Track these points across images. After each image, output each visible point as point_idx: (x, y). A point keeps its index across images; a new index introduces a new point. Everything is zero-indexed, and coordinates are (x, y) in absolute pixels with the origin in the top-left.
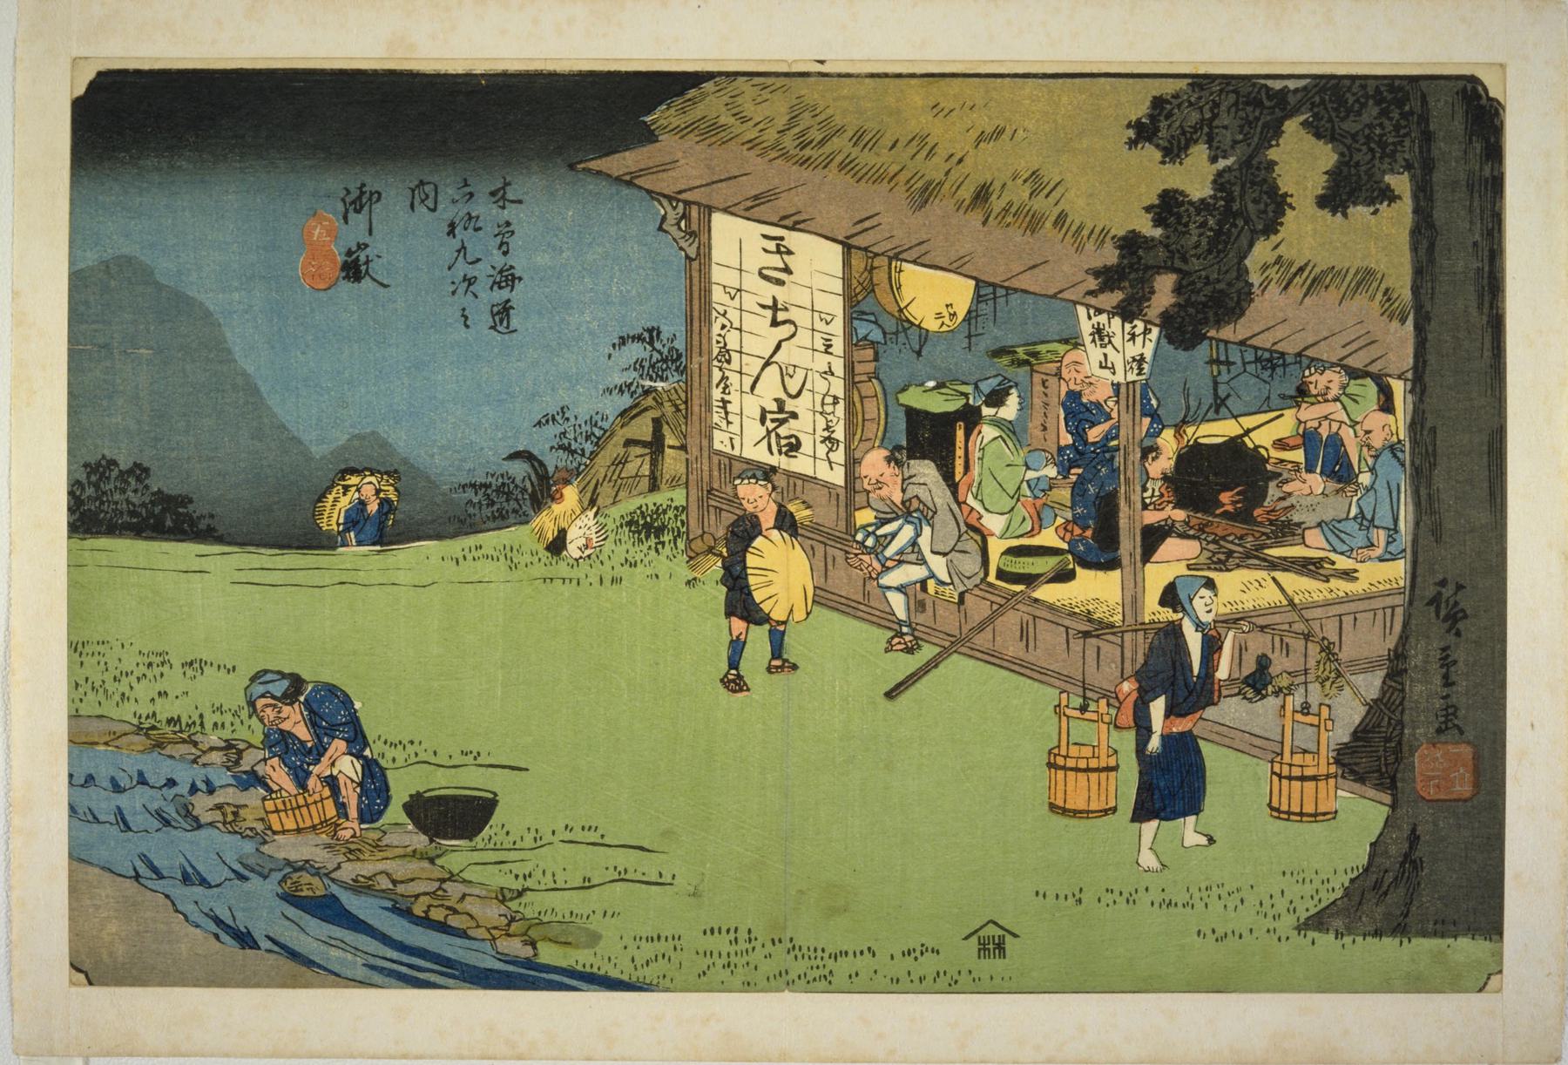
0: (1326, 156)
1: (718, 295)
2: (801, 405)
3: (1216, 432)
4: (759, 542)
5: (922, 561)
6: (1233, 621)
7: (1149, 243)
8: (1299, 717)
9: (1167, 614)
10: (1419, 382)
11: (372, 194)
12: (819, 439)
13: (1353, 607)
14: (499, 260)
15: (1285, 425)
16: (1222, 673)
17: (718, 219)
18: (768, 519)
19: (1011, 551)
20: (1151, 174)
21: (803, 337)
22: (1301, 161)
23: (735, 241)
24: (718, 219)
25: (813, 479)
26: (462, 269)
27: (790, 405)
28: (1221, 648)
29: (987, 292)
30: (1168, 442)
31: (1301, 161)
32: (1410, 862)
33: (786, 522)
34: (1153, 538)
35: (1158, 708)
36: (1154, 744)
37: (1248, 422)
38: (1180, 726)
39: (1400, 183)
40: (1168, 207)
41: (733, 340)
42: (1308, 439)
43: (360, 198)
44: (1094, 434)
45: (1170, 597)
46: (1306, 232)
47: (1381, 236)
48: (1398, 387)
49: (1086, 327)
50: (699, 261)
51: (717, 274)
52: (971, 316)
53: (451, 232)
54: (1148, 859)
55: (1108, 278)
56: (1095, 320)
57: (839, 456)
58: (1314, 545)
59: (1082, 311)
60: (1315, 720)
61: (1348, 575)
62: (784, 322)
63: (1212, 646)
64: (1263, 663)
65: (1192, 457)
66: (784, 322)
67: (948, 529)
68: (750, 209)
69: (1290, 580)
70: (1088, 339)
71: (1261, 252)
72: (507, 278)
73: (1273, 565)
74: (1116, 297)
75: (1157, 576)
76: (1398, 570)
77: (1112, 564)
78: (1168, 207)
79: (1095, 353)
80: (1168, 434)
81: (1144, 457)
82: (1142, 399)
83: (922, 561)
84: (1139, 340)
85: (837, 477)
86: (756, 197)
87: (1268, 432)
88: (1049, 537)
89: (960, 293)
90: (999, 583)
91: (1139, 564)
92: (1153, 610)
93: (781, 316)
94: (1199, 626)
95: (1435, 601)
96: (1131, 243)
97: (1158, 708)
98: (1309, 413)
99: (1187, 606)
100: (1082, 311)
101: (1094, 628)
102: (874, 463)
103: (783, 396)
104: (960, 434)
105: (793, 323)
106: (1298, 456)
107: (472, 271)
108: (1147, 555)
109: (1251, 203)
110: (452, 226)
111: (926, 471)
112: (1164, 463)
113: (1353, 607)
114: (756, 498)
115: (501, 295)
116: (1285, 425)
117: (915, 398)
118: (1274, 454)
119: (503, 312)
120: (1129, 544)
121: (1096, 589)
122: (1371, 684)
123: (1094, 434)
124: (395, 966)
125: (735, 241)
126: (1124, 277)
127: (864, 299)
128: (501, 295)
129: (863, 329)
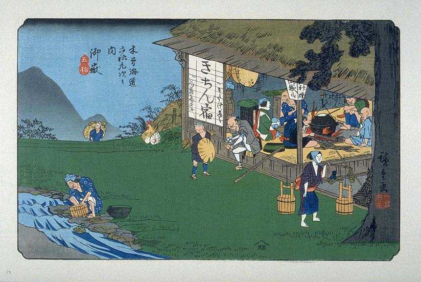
0: (318, 51)
1: (190, 77)
2: (212, 105)
3: (322, 114)
4: (201, 141)
5: (245, 146)
6: (324, 163)
7: (305, 64)
8: (344, 188)
9: (309, 161)
10: (376, 99)
11: (98, 50)
12: (217, 115)
13: (359, 159)
14: (132, 67)
15: (341, 112)
16: (323, 176)
17: (189, 55)
18: (203, 134)
19: (268, 144)
20: (305, 46)
21: (213, 88)
22: (344, 43)
23: (195, 62)
24: (189, 55)
25: (215, 125)
26: (122, 70)
27: (210, 105)
28: (323, 169)
29: (262, 76)
30: (310, 116)
31: (344, 43)
32: (373, 226)
33: (208, 136)
34: (306, 141)
35: (306, 185)
36: (305, 195)
37: (331, 111)
38: (312, 190)
39: (372, 49)
40: (310, 55)
41: (194, 88)
42: (346, 115)
43: (95, 52)
44: (290, 113)
45: (310, 156)
46: (347, 62)
47: (366, 63)
48: (370, 102)
49: (288, 86)
50: (185, 69)
51: (190, 71)
52: (258, 82)
53: (119, 60)
54: (303, 224)
55: (294, 73)
56: (290, 84)
57: (222, 119)
58: (348, 142)
59: (286, 81)
60: (289, 187)
61: (356, 150)
62: (207, 84)
63: (320, 169)
64: (334, 173)
65: (316, 120)
66: (207, 84)
67: (252, 137)
68: (197, 54)
69: (340, 152)
70: (288, 89)
71: (335, 67)
72: (134, 72)
73: (335, 148)
74: (297, 78)
75: (306, 151)
76: (370, 150)
77: (296, 147)
78: (310, 55)
79: (290, 92)
80: (310, 114)
81: (303, 119)
82: (303, 104)
83: (245, 146)
84: (302, 89)
85: (221, 124)
86: (202, 51)
87: (337, 113)
88: (277, 140)
89: (255, 76)
90: (264, 152)
91: (301, 147)
92: (305, 160)
93: (207, 82)
94: (317, 164)
95: (381, 157)
96: (301, 64)
97: (306, 185)
98: (346, 108)
99: (314, 158)
100: (286, 81)
101: (287, 165)
102: (232, 121)
103: (208, 103)
104: (254, 114)
105: (211, 85)
106: (344, 119)
107: (124, 70)
108: (304, 146)
109: (331, 54)
110: (119, 58)
111: (245, 123)
112: (307, 123)
113: (357, 159)
114: (200, 129)
115: (132, 76)
116: (341, 112)
117: (243, 104)
118: (337, 118)
119: (132, 82)
120: (300, 142)
121: (289, 155)
122: (364, 179)
123: (290, 113)
124: (100, 251)
125: (195, 62)
126: (298, 73)
127: (227, 77)
128: (132, 76)
129: (229, 85)
